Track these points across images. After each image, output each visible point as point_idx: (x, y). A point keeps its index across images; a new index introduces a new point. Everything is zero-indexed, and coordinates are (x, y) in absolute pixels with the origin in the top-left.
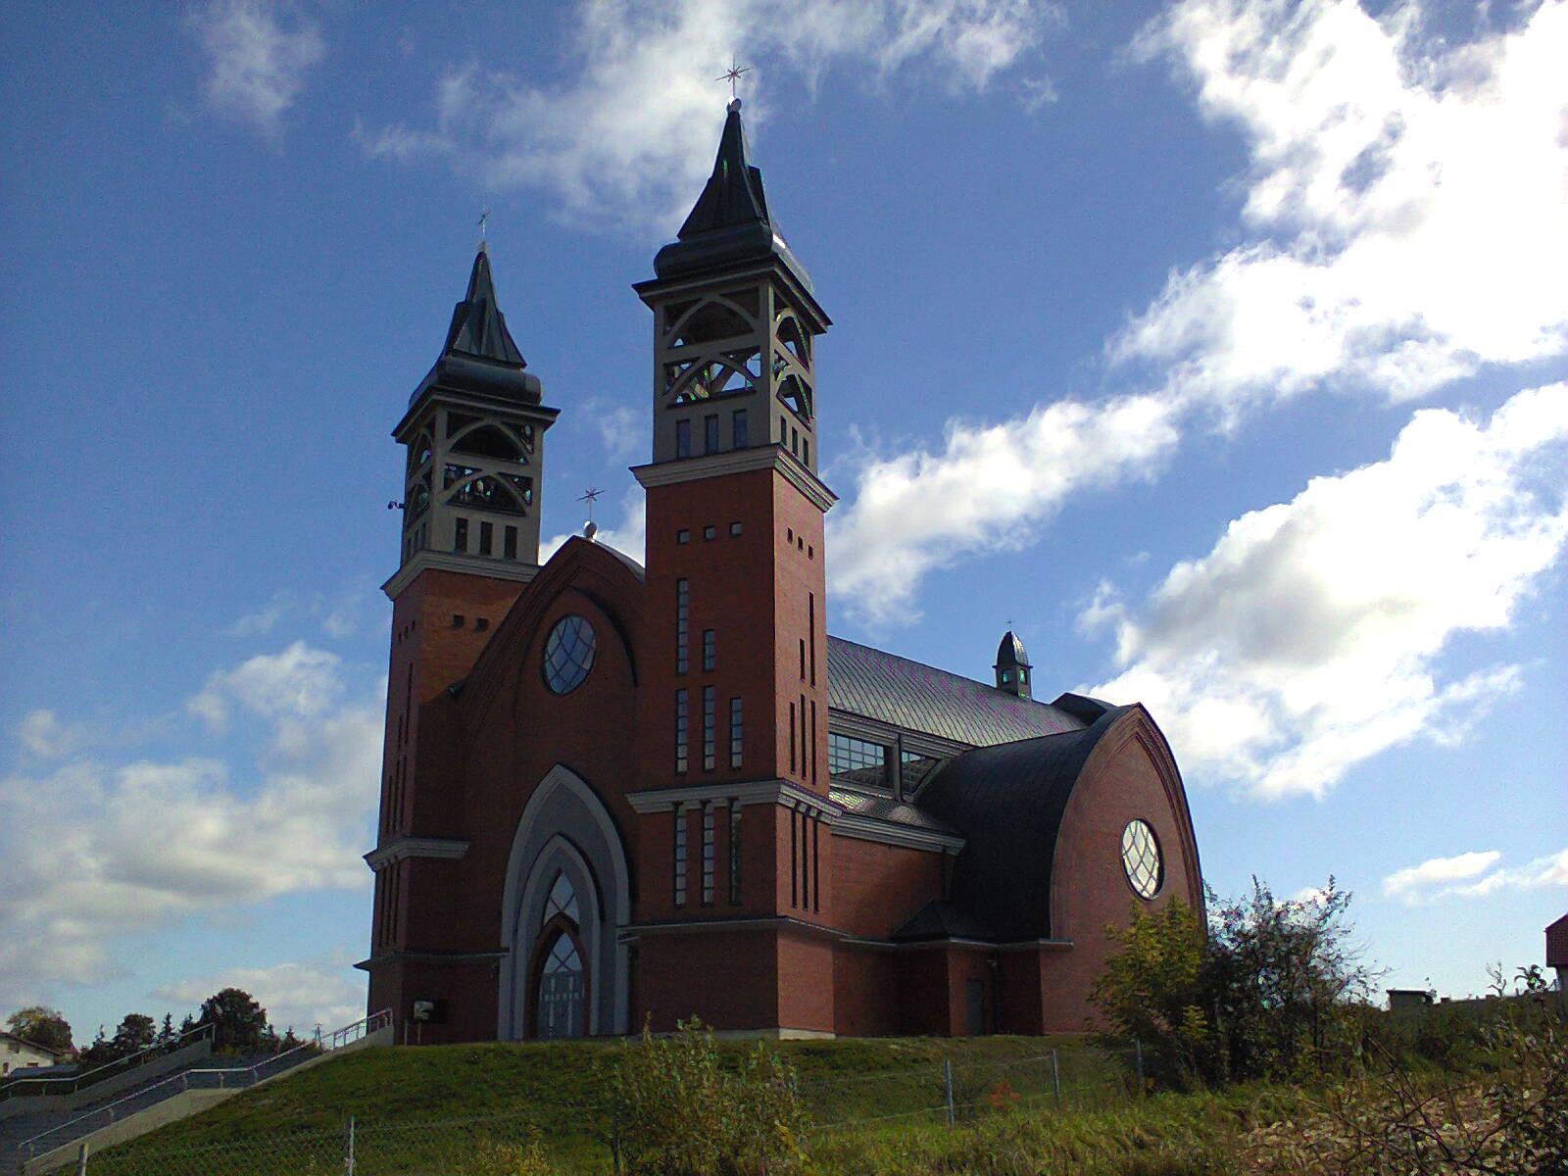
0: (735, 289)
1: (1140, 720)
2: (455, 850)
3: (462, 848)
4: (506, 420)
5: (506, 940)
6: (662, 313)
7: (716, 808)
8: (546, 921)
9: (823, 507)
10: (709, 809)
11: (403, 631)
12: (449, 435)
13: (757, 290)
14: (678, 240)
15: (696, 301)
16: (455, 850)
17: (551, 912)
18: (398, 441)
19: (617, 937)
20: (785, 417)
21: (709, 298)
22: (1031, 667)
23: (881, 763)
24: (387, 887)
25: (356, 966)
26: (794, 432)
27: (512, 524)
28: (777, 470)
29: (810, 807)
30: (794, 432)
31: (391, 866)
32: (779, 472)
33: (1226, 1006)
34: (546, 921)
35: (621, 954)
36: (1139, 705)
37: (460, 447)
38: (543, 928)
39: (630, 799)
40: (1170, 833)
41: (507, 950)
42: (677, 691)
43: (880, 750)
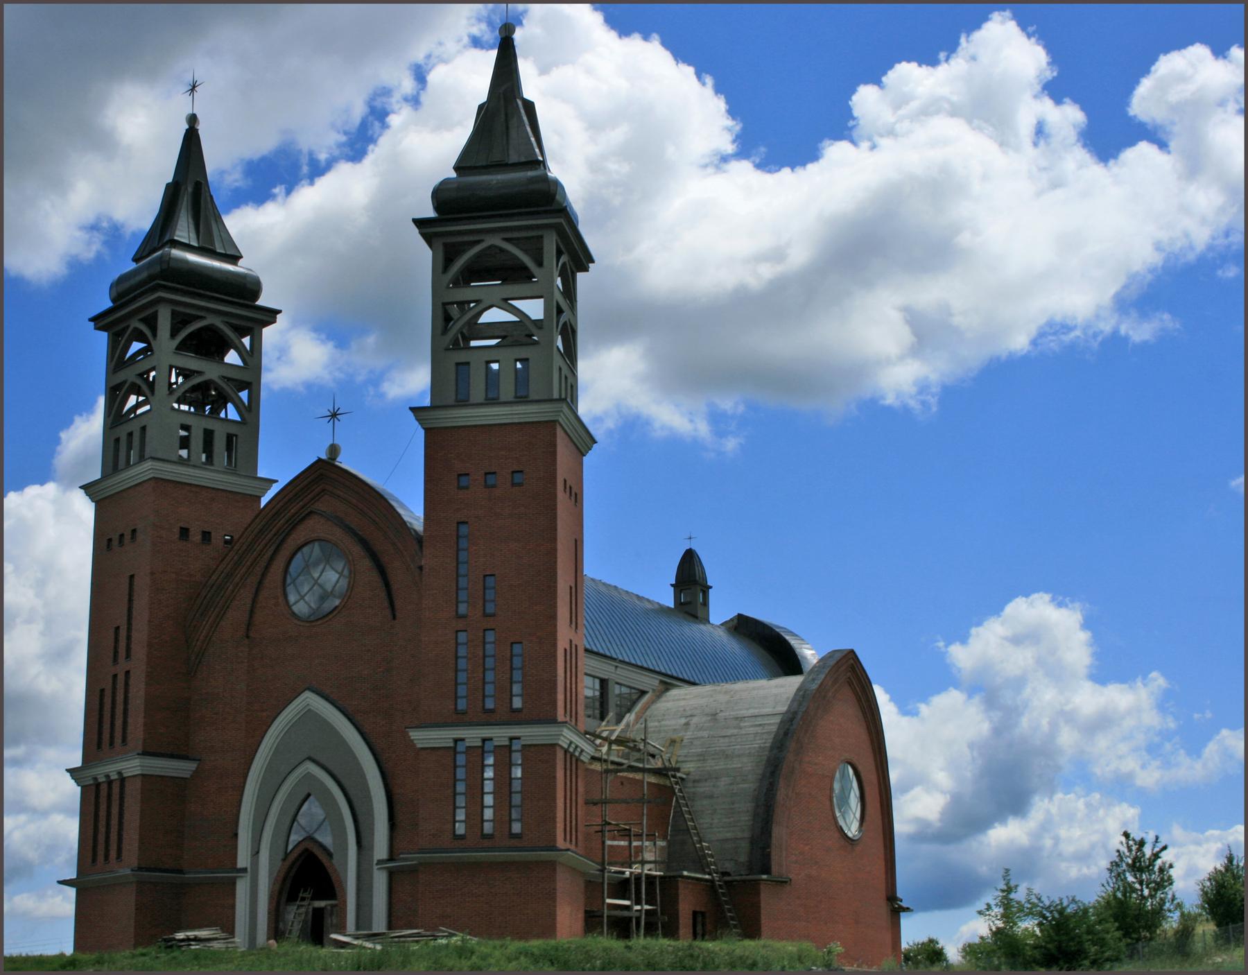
0: (516, 235)
1: (852, 664)
2: (181, 768)
3: (192, 766)
4: (226, 319)
5: (243, 860)
6: (441, 250)
7: (496, 746)
8: (290, 847)
9: (583, 450)
10: (488, 746)
11: (116, 537)
12: (173, 334)
13: (542, 237)
14: (453, 175)
15: (478, 242)
16: (181, 768)
17: (295, 838)
18: (96, 328)
19: (375, 862)
20: (562, 366)
21: (496, 241)
22: (711, 587)
23: (597, 693)
24: (103, 807)
25: (60, 882)
26: (566, 378)
27: (210, 427)
28: (561, 425)
29: (577, 747)
30: (566, 378)
31: (110, 783)
32: (563, 428)
33: (1123, 899)
34: (290, 847)
35: (380, 881)
36: (852, 652)
37: (182, 347)
38: (286, 855)
39: (411, 734)
40: (871, 777)
41: (244, 870)
42: (512, 643)
43: (597, 681)
